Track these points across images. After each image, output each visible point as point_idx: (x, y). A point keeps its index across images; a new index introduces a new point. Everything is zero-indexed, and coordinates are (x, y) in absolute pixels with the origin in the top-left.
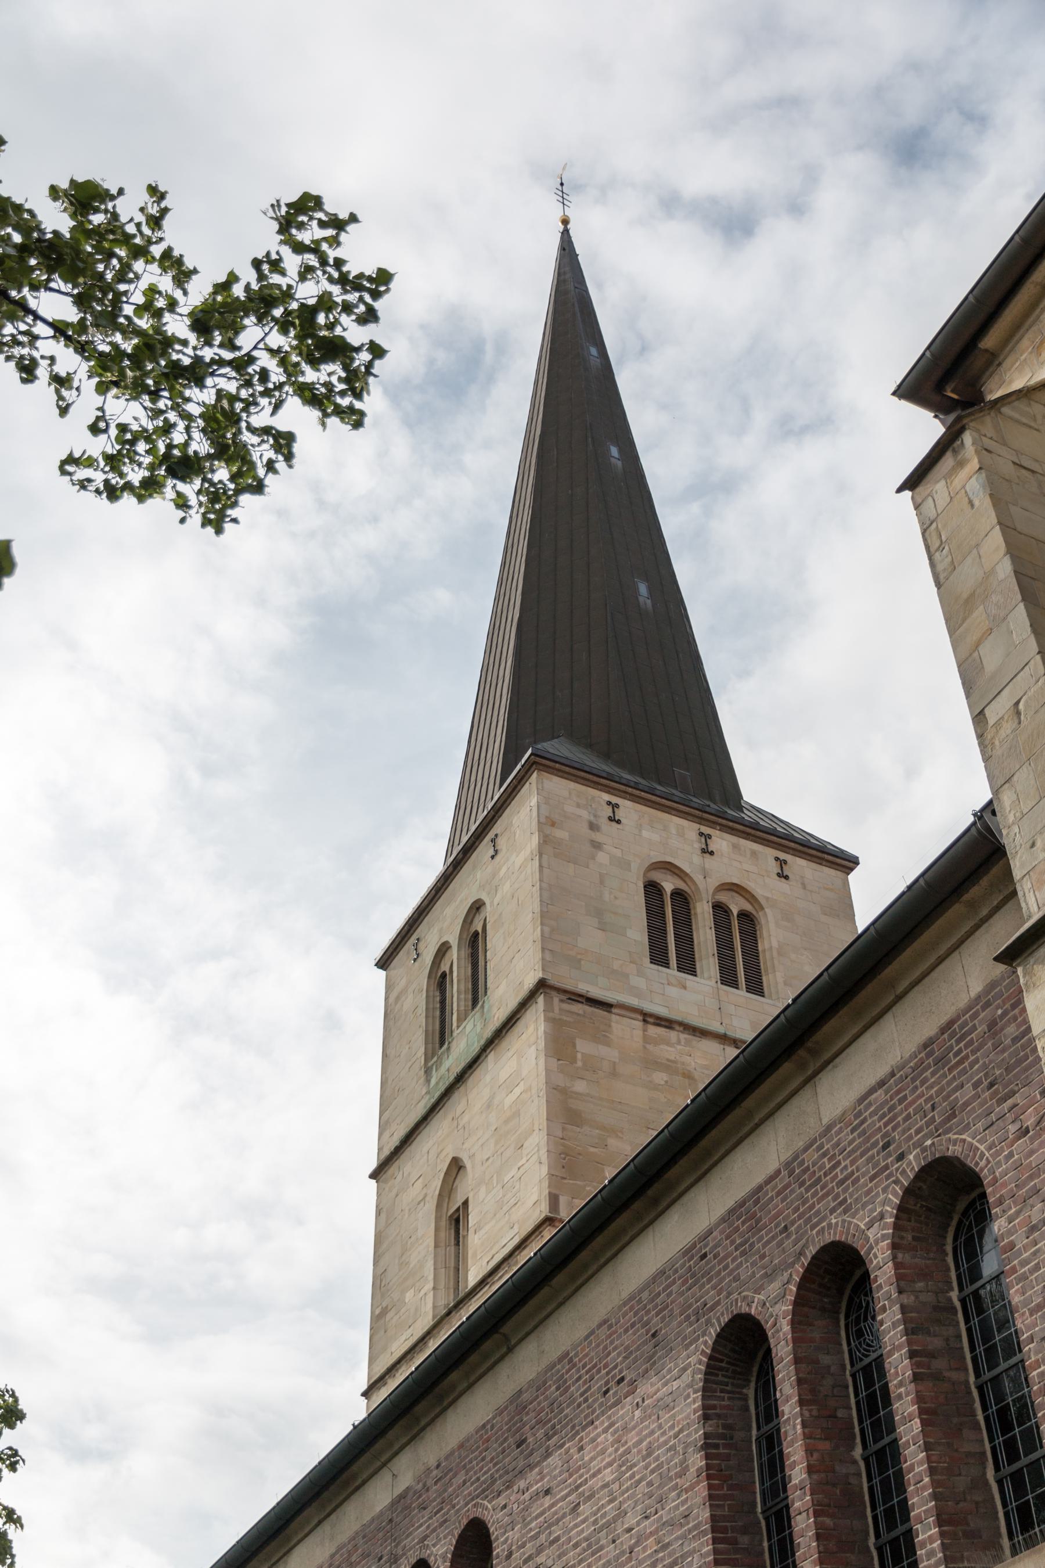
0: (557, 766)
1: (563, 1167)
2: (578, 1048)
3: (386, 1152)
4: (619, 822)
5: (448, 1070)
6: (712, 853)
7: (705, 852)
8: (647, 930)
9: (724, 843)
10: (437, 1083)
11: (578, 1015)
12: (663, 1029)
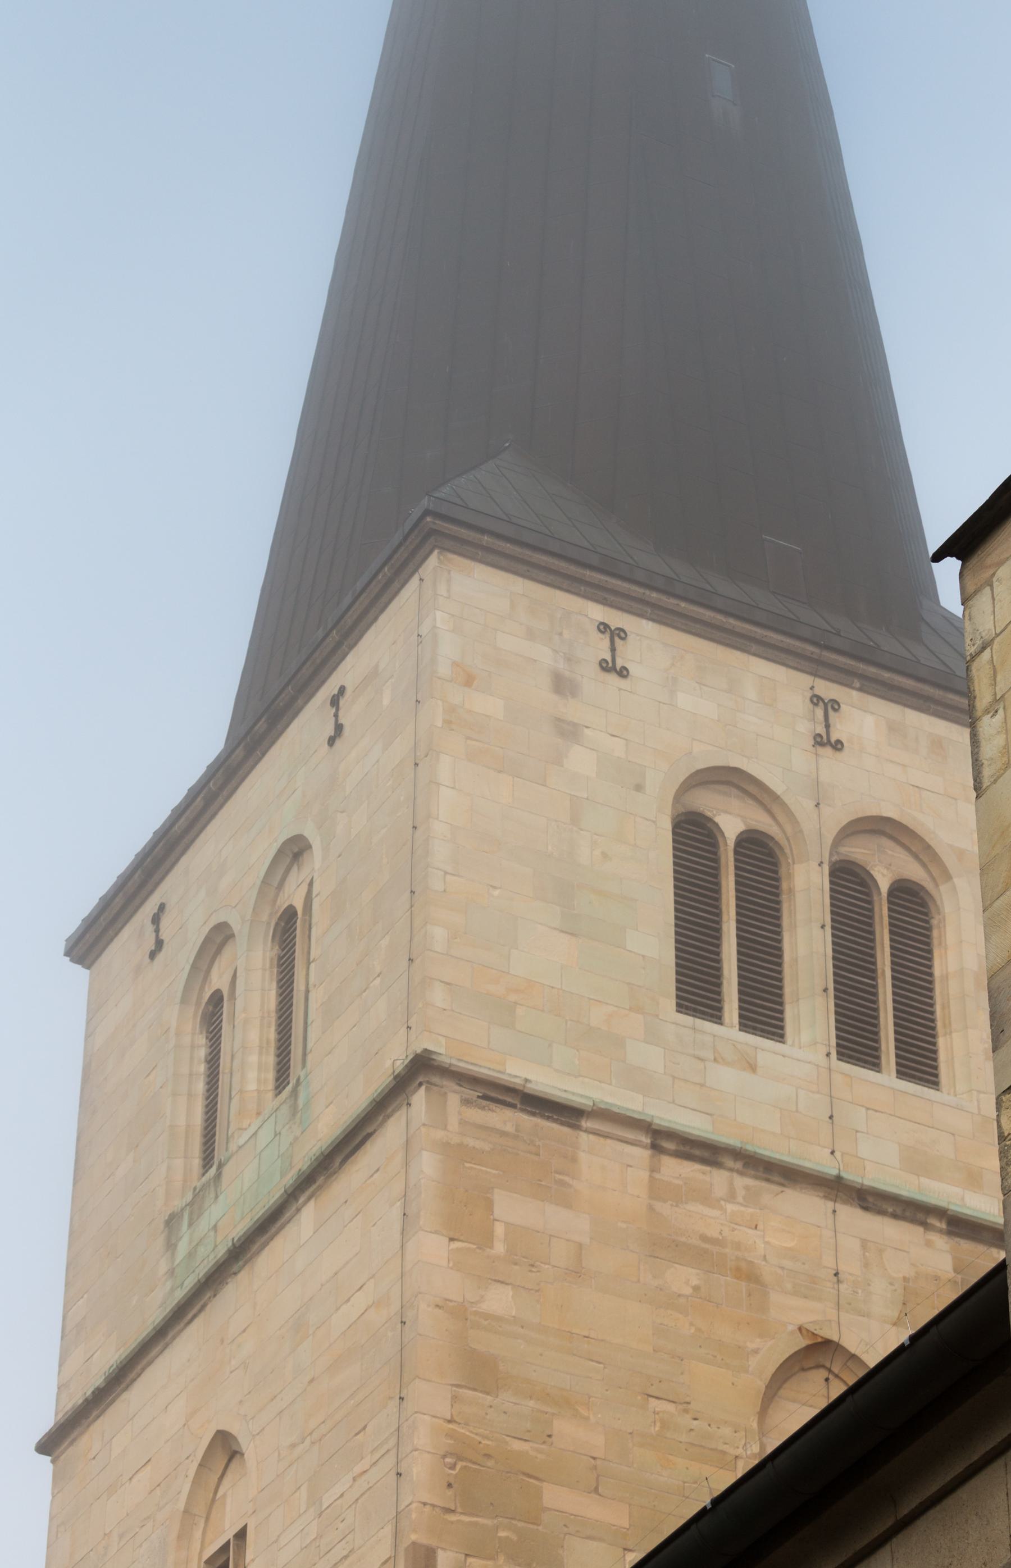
0: (486, 539)
1: (450, 1485)
2: (498, 1212)
3: (77, 1397)
4: (623, 673)
5: (215, 1228)
6: (838, 746)
7: (822, 744)
8: (673, 929)
9: (869, 720)
10: (191, 1255)
11: (503, 1134)
12: (697, 1166)
